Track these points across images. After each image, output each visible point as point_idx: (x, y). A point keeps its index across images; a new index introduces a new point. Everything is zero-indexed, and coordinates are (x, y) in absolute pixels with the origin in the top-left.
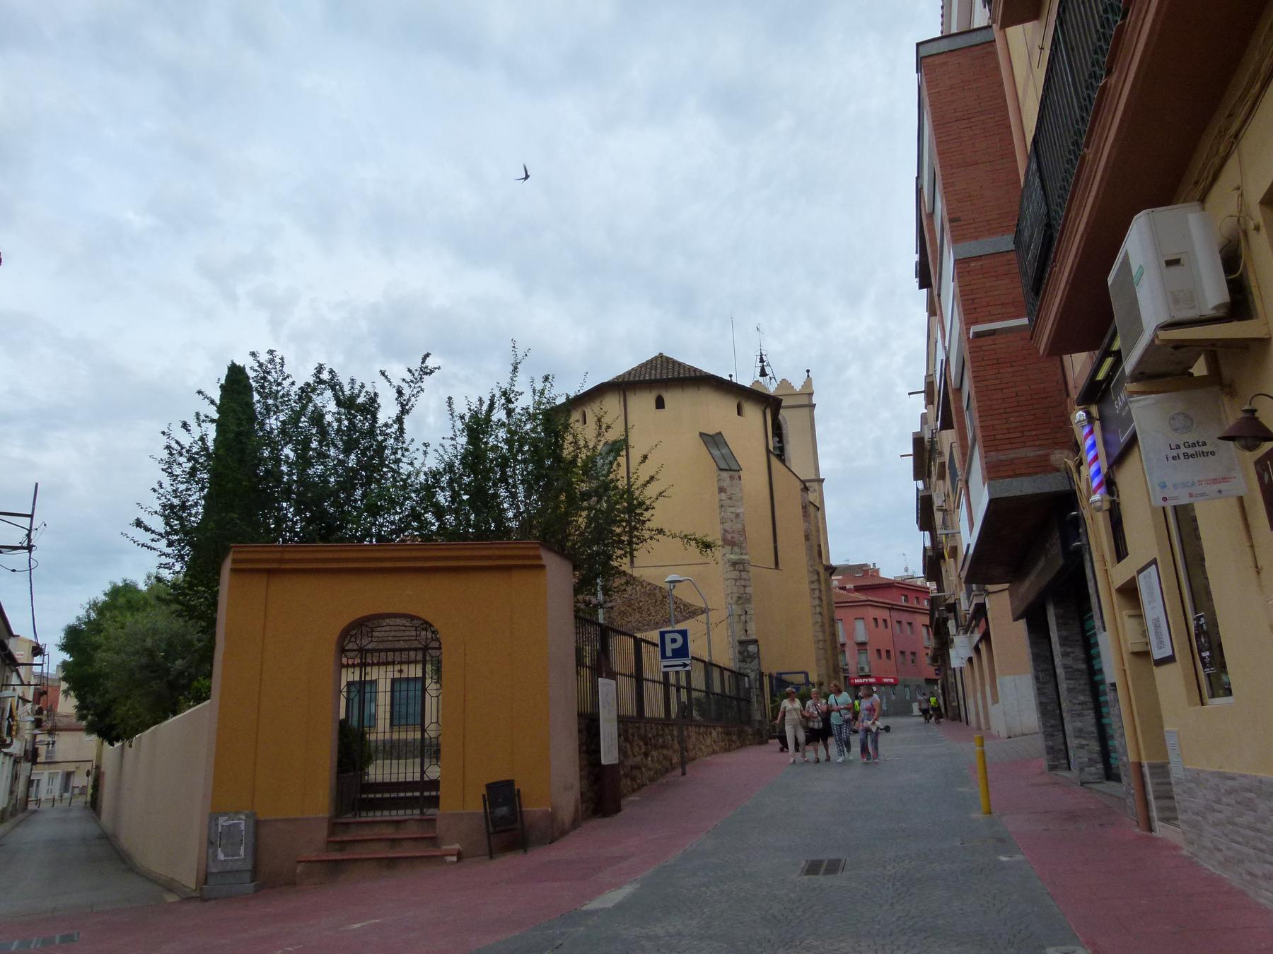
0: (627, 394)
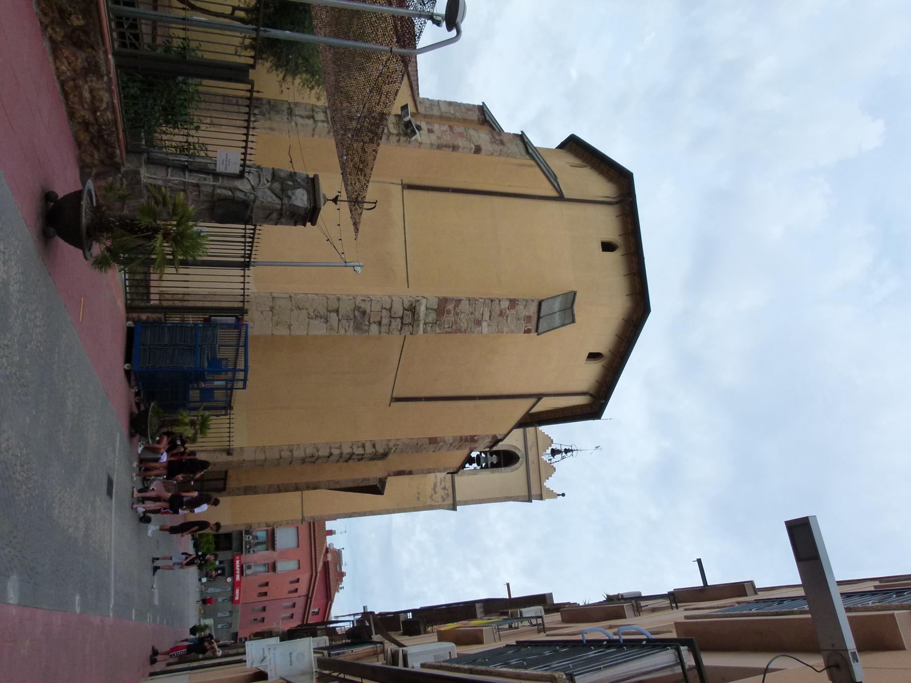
0: (616, 206)
